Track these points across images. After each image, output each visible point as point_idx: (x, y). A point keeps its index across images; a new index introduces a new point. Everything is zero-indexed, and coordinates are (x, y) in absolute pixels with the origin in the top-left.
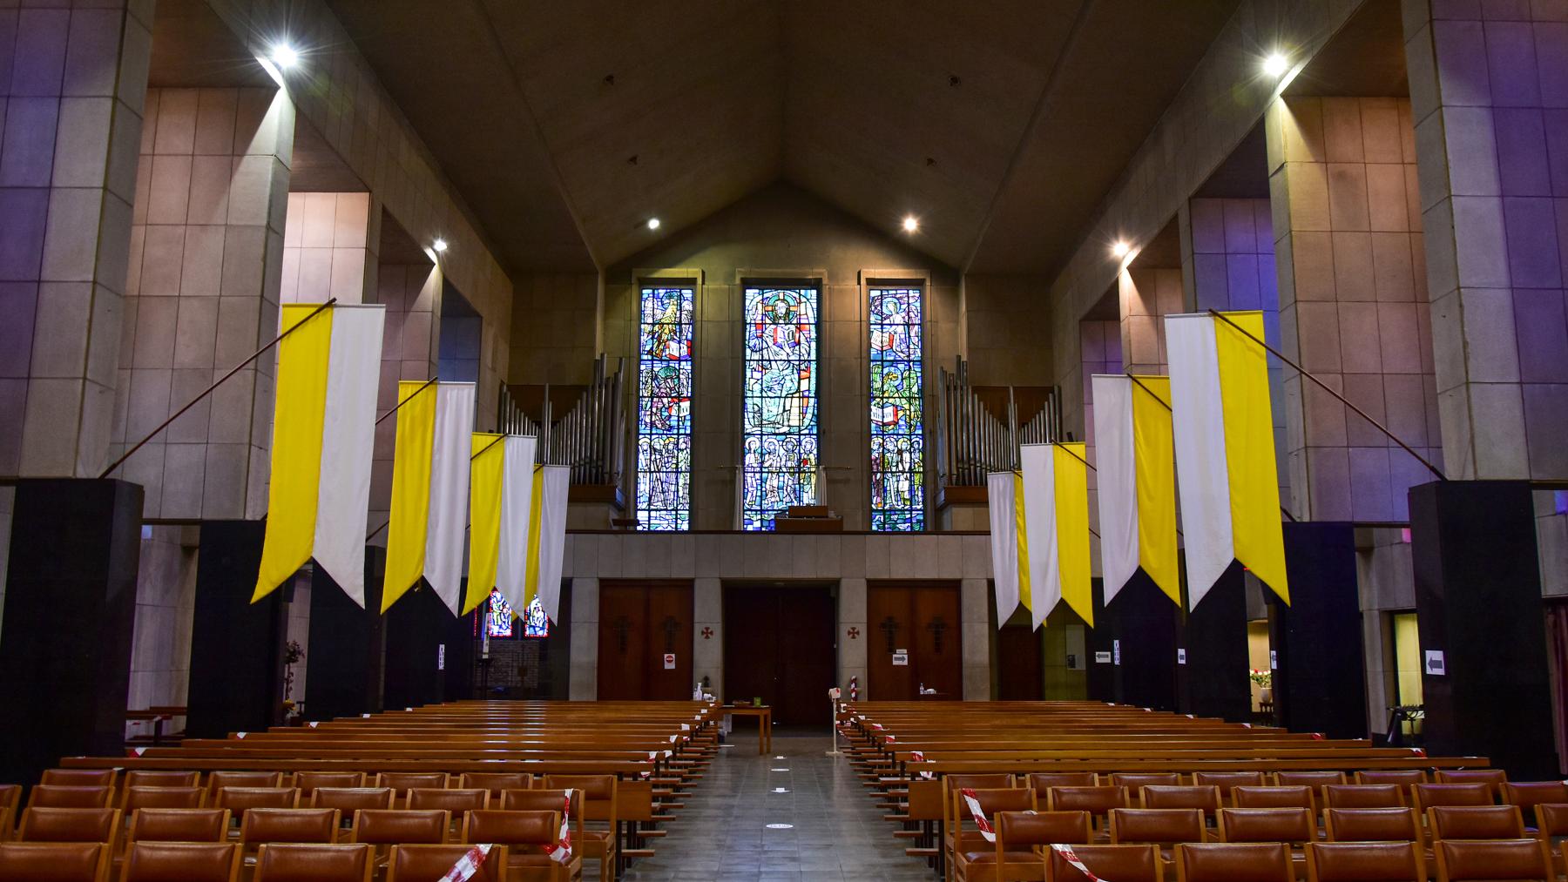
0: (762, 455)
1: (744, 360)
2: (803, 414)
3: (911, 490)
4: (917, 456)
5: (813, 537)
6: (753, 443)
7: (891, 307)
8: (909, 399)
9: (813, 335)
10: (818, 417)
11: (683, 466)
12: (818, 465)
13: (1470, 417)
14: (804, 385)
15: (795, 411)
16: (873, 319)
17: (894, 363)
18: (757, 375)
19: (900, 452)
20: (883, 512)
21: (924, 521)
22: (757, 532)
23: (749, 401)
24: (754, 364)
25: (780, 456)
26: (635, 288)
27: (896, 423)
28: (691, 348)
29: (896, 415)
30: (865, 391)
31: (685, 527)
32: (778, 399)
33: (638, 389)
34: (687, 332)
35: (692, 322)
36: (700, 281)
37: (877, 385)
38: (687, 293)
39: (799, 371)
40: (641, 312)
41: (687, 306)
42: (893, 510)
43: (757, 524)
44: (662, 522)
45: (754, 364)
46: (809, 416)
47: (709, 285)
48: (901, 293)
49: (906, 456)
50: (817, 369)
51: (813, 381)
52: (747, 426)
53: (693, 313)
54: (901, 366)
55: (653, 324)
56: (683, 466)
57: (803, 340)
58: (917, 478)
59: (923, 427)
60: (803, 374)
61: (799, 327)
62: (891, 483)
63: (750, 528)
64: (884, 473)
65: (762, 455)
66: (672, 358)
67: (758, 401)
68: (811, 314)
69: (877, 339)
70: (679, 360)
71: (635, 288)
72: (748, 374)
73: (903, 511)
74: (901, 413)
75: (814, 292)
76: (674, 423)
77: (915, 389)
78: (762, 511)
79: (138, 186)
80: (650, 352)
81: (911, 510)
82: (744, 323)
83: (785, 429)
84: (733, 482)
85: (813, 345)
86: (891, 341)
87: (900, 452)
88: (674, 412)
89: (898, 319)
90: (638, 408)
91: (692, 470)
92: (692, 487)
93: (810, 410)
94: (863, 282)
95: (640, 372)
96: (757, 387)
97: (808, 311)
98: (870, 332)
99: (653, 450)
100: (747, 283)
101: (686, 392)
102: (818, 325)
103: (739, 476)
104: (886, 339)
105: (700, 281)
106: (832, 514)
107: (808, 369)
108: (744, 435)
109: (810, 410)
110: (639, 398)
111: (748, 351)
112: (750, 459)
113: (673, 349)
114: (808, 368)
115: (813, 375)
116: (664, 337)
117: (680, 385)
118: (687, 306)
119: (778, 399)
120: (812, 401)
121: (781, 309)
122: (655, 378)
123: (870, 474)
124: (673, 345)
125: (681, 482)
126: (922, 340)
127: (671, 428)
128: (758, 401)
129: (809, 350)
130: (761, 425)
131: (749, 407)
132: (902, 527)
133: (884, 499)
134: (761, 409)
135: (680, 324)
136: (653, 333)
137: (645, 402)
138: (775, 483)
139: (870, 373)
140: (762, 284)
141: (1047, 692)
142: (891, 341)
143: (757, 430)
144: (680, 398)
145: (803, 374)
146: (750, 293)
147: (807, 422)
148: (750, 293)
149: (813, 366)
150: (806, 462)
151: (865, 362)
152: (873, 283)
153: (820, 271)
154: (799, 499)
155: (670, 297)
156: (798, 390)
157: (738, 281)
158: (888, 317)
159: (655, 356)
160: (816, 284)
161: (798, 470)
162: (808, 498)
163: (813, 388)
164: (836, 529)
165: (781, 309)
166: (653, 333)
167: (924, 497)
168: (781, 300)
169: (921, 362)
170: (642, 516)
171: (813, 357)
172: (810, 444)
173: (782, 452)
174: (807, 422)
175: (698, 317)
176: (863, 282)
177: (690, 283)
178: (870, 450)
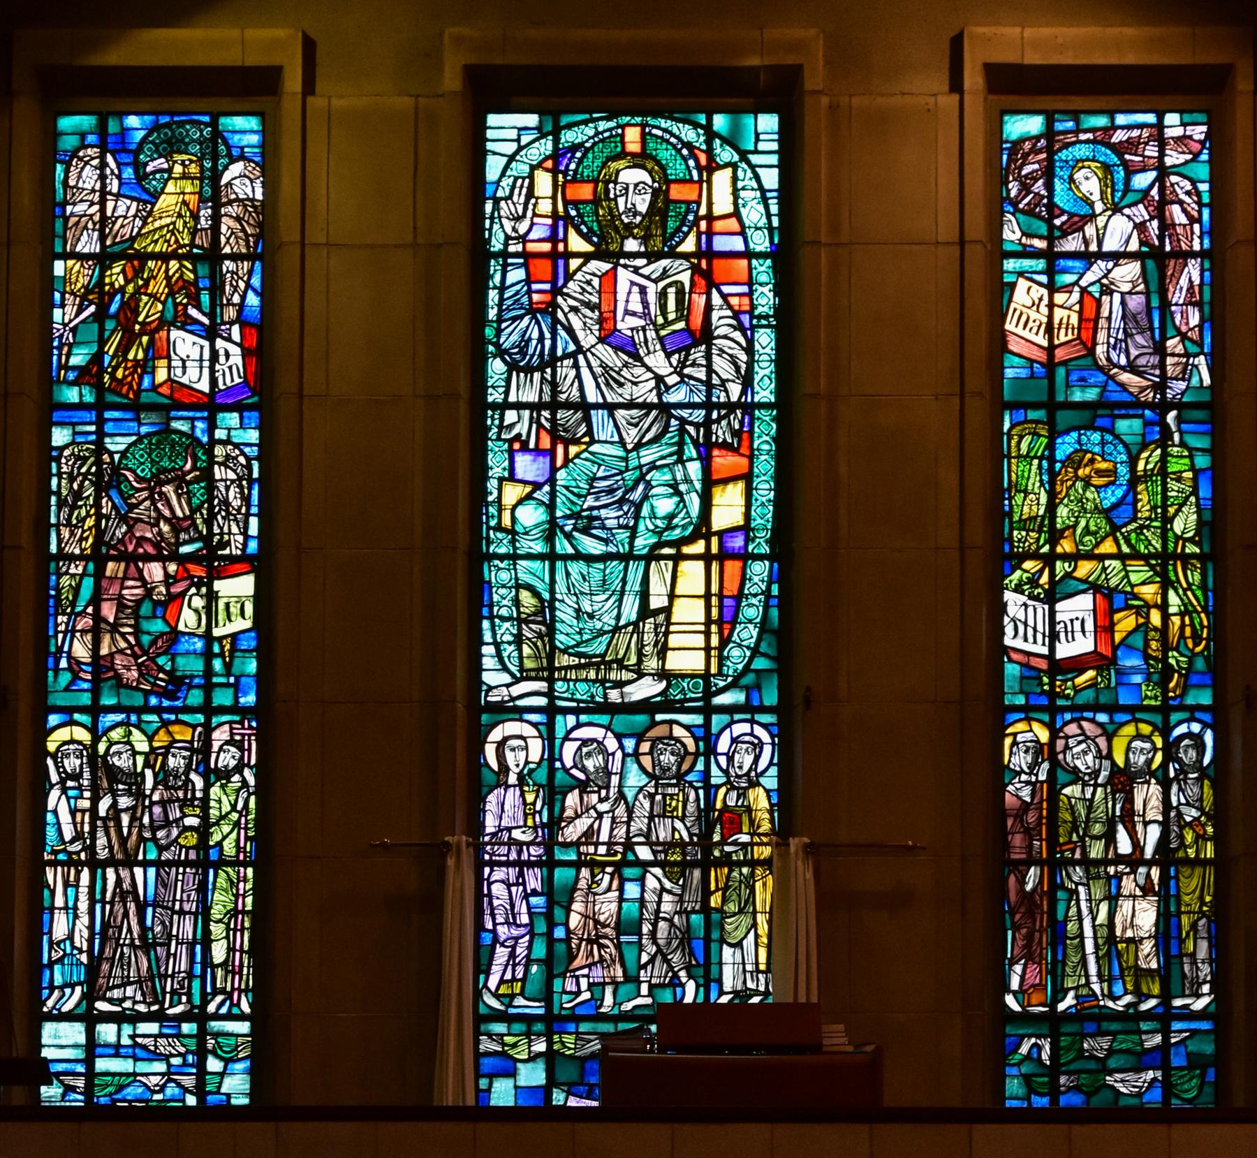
0: (553, 794)
1: (479, 405)
2: (723, 619)
3: (1166, 932)
4: (1191, 801)
5: (757, 1132)
6: (516, 744)
7: (1090, 185)
8: (1163, 564)
9: (765, 299)
10: (782, 636)
11: (227, 839)
12: (781, 835)
13: (416, 153)
14: (728, 508)
15: (689, 611)
16: (1011, 234)
17: (1100, 414)
18: (527, 466)
19: (1123, 781)
20: (1052, 1023)
21: (1220, 1059)
22: (535, 1112)
23: (499, 575)
24: (517, 421)
25: (624, 800)
26: (25, 109)
27: (1100, 661)
28: (258, 353)
29: (1105, 628)
30: (978, 533)
31: (236, 1086)
32: (626, 575)
33: (42, 528)
34: (245, 290)
35: (264, 250)
36: (293, 82)
37: (1031, 504)
38: (244, 129)
39: (705, 453)
40: (50, 208)
41: (242, 181)
42: (1090, 1017)
43: (532, 1075)
44: (143, 1070)
45: (517, 421)
46: (747, 634)
47: (337, 96)
48: (1131, 122)
49: (1147, 796)
50: (784, 443)
51: (765, 491)
52: (492, 677)
53: (265, 212)
54: (1128, 427)
55: (103, 259)
56: (227, 839)
57: (721, 320)
58: (1191, 885)
59: (1217, 676)
60: (723, 462)
61: (707, 266)
62: (1086, 917)
63: (502, 1094)
64: (1054, 865)
65: (553, 794)
66: (180, 398)
67: (531, 571)
68: (753, 214)
69: (1030, 315)
70: (212, 404)
71: (25, 109)
72: (497, 463)
73: (1131, 1017)
74: (1126, 623)
75: (769, 122)
76: (191, 665)
77: (1185, 522)
78: (553, 1022)
79: (205, 100)
80: (89, 374)
81: (1164, 1017)
82: (479, 254)
83: (646, 689)
84: (431, 901)
85: (765, 339)
86: (1090, 321)
87: (1123, 781)
88: (188, 620)
89: (1118, 232)
90: (44, 604)
91: (268, 849)
92: (266, 927)
93: (751, 611)
94: (973, 79)
95: (48, 454)
96: (531, 516)
97: (741, 197)
98: (1001, 292)
99: (104, 776)
100: (493, 89)
101: (243, 535)
102: (784, 257)
103: (458, 878)
104: (1067, 316)
105: (293, 82)
106: (836, 1037)
107: (742, 441)
108: (481, 713)
109: (751, 611)
110: (45, 563)
111: (497, 367)
112: (503, 810)
113: (188, 359)
114: (743, 436)
115: (765, 466)
116: (149, 311)
117: (213, 505)
118: (242, 181)
119: (626, 575)
120: (759, 570)
121: (634, 188)
122: (108, 479)
123: (999, 870)
124: (186, 344)
125: (220, 902)
126: (1215, 317)
127: (178, 683)
128: (531, 571)
129: (745, 361)
130: (548, 672)
131: (502, 599)
132: (1125, 1084)
133: (1056, 971)
134: (546, 608)
135: (213, 256)
136: (98, 294)
137: (73, 578)
138: (607, 908)
139: (997, 456)
140: (553, 92)
141: (991, 97)
142: (1090, 321)
143: (530, 692)
144: (214, 563)
145: (723, 462)
146: (504, 127)
147: (737, 656)
148: (504, 127)
149: (765, 431)
150: (733, 820)
151: (977, 411)
152: (1015, 84)
153: (799, 39)
154: (708, 976)
155: (170, 147)
156: (702, 528)
157: (452, 80)
158: (1077, 223)
159: (113, 393)
160: (777, 91)
161: (696, 859)
162: (741, 966)
163: (763, 516)
164: (851, 1095)
165: (634, 188)
166: (98, 294)
167: (1219, 959)
168: (632, 161)
169: (1212, 410)
170: (60, 1040)
171: (765, 392)
172: (749, 751)
173: (635, 779)
174: (737, 656)
175: (288, 230)
176: (973, 79)
177: (251, 86)
178: (1000, 773)
